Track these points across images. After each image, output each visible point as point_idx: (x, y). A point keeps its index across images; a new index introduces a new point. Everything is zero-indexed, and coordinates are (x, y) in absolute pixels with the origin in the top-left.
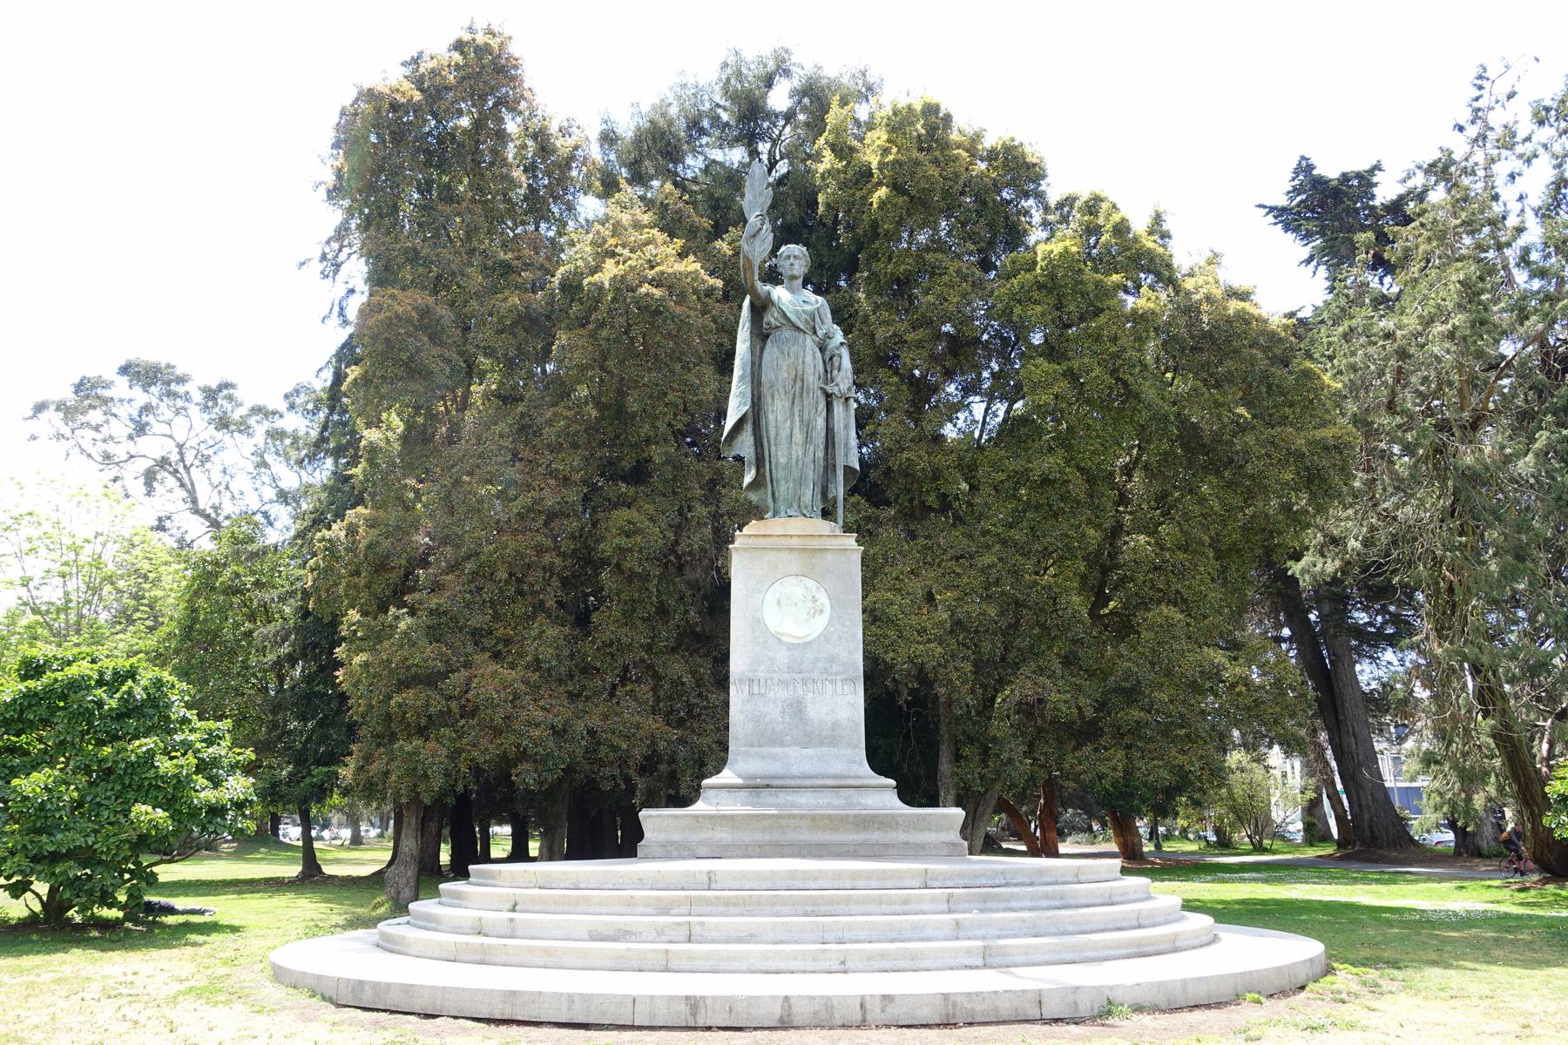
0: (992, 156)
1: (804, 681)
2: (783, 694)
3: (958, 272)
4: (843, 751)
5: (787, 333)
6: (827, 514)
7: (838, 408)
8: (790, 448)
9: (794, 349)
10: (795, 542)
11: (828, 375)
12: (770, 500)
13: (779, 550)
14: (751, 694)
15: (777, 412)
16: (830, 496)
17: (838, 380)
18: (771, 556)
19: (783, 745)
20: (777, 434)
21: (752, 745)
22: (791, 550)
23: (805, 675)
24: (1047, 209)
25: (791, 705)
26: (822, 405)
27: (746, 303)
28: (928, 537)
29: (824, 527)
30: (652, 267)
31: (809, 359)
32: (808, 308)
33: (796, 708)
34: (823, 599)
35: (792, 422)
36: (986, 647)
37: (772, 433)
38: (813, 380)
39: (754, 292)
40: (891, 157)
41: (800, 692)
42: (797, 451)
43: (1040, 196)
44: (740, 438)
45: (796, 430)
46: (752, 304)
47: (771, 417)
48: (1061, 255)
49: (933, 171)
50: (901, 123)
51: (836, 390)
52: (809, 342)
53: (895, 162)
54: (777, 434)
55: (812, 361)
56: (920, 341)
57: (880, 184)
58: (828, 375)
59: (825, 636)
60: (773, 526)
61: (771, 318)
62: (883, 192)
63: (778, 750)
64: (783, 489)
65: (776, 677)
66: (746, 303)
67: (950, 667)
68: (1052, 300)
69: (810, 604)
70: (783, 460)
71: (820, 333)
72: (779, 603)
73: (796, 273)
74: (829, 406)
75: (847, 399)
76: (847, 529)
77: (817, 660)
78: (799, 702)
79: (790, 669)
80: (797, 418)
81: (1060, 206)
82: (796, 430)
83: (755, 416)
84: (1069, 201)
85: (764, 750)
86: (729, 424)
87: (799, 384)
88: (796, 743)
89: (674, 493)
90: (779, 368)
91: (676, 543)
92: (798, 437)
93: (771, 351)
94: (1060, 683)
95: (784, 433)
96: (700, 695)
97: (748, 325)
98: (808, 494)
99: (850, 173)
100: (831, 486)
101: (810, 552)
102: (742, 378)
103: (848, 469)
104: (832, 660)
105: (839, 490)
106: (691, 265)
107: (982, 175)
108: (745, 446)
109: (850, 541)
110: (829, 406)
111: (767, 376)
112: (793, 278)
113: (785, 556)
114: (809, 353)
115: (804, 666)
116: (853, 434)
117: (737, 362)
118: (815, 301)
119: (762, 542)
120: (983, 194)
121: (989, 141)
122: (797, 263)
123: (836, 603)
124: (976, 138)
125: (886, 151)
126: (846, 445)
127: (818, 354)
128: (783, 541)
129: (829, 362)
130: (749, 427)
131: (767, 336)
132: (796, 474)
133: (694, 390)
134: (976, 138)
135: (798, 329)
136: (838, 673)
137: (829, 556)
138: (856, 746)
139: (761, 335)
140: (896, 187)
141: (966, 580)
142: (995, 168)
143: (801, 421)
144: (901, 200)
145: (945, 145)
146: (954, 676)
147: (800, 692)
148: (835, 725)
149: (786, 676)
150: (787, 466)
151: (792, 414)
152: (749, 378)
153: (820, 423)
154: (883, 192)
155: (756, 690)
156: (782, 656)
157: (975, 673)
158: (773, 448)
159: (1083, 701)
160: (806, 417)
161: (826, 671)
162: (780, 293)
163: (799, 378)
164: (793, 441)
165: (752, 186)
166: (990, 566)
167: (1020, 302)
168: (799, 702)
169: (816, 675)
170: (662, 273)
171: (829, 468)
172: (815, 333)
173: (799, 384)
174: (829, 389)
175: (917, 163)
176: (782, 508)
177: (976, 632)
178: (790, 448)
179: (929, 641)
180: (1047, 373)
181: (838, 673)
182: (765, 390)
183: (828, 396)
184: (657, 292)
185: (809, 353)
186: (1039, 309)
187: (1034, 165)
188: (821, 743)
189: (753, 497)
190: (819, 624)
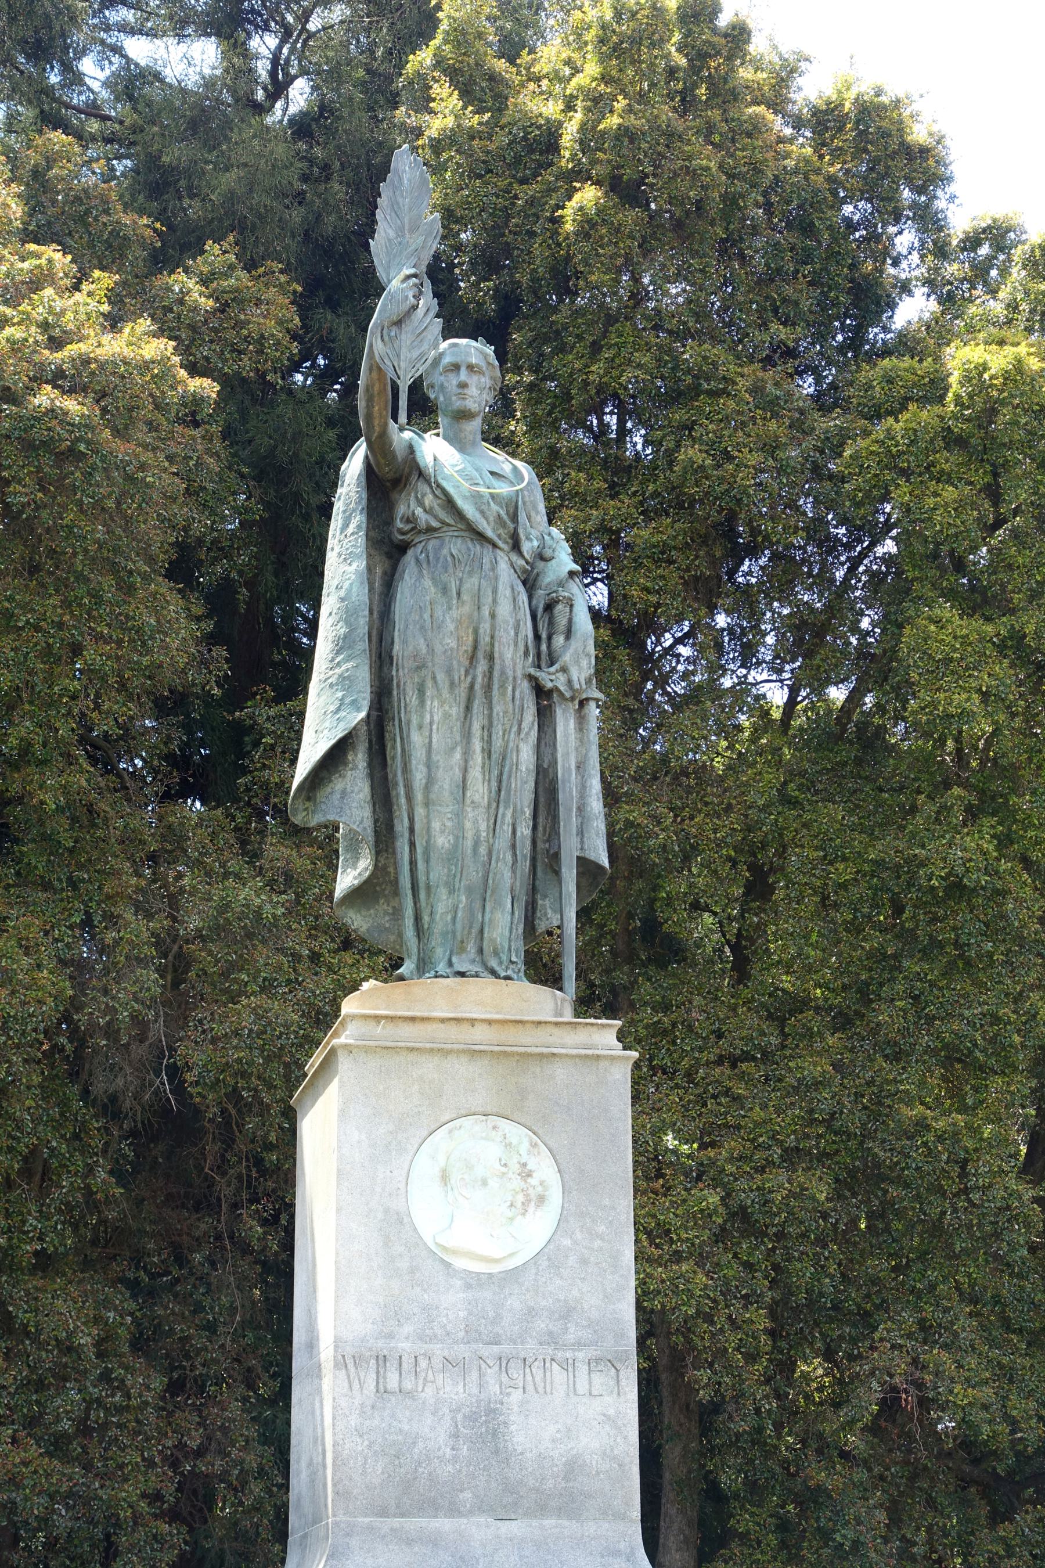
0: (825, 121)
1: (503, 1363)
2: (454, 1391)
3: (756, 390)
4: (591, 1528)
5: (456, 546)
6: (542, 970)
7: (565, 723)
8: (459, 816)
9: (471, 583)
10: (480, 1035)
11: (543, 650)
12: (410, 933)
13: (445, 1053)
14: (382, 1391)
15: (431, 726)
16: (542, 927)
17: (567, 658)
18: (428, 1068)
19: (454, 1511)
20: (430, 781)
21: (383, 1513)
22: (473, 1054)
23: (505, 1348)
24: (941, 251)
25: (472, 1418)
26: (530, 715)
27: (354, 466)
28: (665, 1007)
29: (545, 1003)
30: (56, 343)
31: (504, 609)
32: (503, 489)
33: (486, 1427)
34: (545, 1170)
35: (467, 754)
36: (802, 1272)
37: (419, 777)
38: (512, 657)
39: (380, 446)
40: (613, 121)
41: (494, 1388)
42: (476, 822)
43: (928, 221)
44: (338, 784)
45: (476, 773)
46: (370, 471)
47: (417, 739)
48: (1007, 376)
49: (708, 159)
50: (636, 41)
51: (561, 682)
52: (505, 569)
53: (624, 133)
54: (430, 781)
55: (510, 613)
56: (665, 548)
57: (579, 175)
58: (543, 650)
59: (549, 1258)
60: (432, 996)
61: (414, 507)
62: (588, 196)
63: (444, 1524)
64: (442, 906)
65: (438, 1350)
66: (354, 466)
67: (721, 1321)
68: (980, 477)
69: (517, 1183)
70: (442, 841)
71: (527, 547)
72: (445, 1177)
73: (472, 405)
74: (545, 715)
75: (582, 703)
76: (587, 1004)
77: (531, 1313)
78: (491, 1412)
79: (472, 1334)
80: (477, 745)
81: (972, 242)
82: (476, 773)
83: (378, 735)
84: (998, 235)
85: (413, 1524)
86: (312, 750)
87: (482, 667)
88: (482, 1507)
89: (73, 884)
90: (437, 626)
91: (75, 1004)
92: (479, 790)
93: (414, 588)
94: (972, 1361)
95: (446, 781)
96: (106, 1377)
97: (358, 519)
98: (503, 925)
99: (502, 139)
100: (545, 904)
101: (514, 1060)
102: (344, 645)
103: (586, 867)
104: (566, 1313)
105: (565, 913)
106: (140, 343)
107: (805, 169)
108: (351, 804)
109: (603, 1035)
110: (545, 715)
111: (406, 645)
112: (463, 415)
113: (462, 1068)
114: (504, 592)
115: (500, 1330)
116: (595, 785)
117: (330, 605)
118: (514, 476)
119: (407, 1033)
120: (804, 216)
121: (811, 89)
122: (473, 381)
123: (574, 1180)
124: (785, 74)
125: (598, 104)
126: (581, 809)
127: (523, 597)
128: (453, 1032)
129: (546, 615)
130: (359, 758)
131: (402, 548)
132: (473, 874)
133: (141, 639)
134: (785, 74)
135: (480, 536)
136: (579, 1345)
137: (560, 1072)
138: (622, 1517)
139: (390, 548)
140: (624, 190)
141: (758, 1114)
142: (837, 154)
143: (488, 752)
144: (630, 217)
145: (726, 94)
146: (731, 1340)
147: (494, 1388)
148: (573, 1467)
149: (462, 1351)
150: (453, 856)
151: (467, 735)
152: (363, 645)
153: (526, 756)
154: (588, 196)
155: (392, 1380)
156: (453, 1303)
157: (772, 1333)
158: (420, 811)
159: (1019, 1406)
160: (498, 743)
161: (552, 1339)
162: (434, 450)
163: (481, 652)
164: (464, 795)
165: (394, 205)
166: (817, 1085)
167: (905, 473)
168: (491, 1412)
169: (530, 1348)
170: (86, 361)
171: (544, 859)
172: (516, 546)
173: (482, 667)
174: (549, 678)
175: (671, 136)
176: (440, 953)
177: (780, 1236)
178: (459, 816)
179: (677, 1257)
180: (965, 640)
181: (579, 1345)
182: (404, 676)
183: (541, 693)
184: (71, 405)
185: (504, 592)
186: (950, 493)
187: (924, 151)
188: (541, 1509)
189: (358, 921)
190: (537, 1229)
